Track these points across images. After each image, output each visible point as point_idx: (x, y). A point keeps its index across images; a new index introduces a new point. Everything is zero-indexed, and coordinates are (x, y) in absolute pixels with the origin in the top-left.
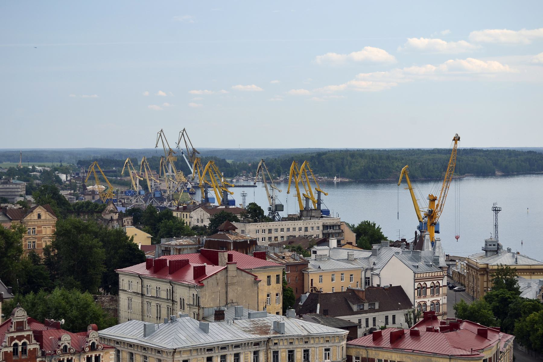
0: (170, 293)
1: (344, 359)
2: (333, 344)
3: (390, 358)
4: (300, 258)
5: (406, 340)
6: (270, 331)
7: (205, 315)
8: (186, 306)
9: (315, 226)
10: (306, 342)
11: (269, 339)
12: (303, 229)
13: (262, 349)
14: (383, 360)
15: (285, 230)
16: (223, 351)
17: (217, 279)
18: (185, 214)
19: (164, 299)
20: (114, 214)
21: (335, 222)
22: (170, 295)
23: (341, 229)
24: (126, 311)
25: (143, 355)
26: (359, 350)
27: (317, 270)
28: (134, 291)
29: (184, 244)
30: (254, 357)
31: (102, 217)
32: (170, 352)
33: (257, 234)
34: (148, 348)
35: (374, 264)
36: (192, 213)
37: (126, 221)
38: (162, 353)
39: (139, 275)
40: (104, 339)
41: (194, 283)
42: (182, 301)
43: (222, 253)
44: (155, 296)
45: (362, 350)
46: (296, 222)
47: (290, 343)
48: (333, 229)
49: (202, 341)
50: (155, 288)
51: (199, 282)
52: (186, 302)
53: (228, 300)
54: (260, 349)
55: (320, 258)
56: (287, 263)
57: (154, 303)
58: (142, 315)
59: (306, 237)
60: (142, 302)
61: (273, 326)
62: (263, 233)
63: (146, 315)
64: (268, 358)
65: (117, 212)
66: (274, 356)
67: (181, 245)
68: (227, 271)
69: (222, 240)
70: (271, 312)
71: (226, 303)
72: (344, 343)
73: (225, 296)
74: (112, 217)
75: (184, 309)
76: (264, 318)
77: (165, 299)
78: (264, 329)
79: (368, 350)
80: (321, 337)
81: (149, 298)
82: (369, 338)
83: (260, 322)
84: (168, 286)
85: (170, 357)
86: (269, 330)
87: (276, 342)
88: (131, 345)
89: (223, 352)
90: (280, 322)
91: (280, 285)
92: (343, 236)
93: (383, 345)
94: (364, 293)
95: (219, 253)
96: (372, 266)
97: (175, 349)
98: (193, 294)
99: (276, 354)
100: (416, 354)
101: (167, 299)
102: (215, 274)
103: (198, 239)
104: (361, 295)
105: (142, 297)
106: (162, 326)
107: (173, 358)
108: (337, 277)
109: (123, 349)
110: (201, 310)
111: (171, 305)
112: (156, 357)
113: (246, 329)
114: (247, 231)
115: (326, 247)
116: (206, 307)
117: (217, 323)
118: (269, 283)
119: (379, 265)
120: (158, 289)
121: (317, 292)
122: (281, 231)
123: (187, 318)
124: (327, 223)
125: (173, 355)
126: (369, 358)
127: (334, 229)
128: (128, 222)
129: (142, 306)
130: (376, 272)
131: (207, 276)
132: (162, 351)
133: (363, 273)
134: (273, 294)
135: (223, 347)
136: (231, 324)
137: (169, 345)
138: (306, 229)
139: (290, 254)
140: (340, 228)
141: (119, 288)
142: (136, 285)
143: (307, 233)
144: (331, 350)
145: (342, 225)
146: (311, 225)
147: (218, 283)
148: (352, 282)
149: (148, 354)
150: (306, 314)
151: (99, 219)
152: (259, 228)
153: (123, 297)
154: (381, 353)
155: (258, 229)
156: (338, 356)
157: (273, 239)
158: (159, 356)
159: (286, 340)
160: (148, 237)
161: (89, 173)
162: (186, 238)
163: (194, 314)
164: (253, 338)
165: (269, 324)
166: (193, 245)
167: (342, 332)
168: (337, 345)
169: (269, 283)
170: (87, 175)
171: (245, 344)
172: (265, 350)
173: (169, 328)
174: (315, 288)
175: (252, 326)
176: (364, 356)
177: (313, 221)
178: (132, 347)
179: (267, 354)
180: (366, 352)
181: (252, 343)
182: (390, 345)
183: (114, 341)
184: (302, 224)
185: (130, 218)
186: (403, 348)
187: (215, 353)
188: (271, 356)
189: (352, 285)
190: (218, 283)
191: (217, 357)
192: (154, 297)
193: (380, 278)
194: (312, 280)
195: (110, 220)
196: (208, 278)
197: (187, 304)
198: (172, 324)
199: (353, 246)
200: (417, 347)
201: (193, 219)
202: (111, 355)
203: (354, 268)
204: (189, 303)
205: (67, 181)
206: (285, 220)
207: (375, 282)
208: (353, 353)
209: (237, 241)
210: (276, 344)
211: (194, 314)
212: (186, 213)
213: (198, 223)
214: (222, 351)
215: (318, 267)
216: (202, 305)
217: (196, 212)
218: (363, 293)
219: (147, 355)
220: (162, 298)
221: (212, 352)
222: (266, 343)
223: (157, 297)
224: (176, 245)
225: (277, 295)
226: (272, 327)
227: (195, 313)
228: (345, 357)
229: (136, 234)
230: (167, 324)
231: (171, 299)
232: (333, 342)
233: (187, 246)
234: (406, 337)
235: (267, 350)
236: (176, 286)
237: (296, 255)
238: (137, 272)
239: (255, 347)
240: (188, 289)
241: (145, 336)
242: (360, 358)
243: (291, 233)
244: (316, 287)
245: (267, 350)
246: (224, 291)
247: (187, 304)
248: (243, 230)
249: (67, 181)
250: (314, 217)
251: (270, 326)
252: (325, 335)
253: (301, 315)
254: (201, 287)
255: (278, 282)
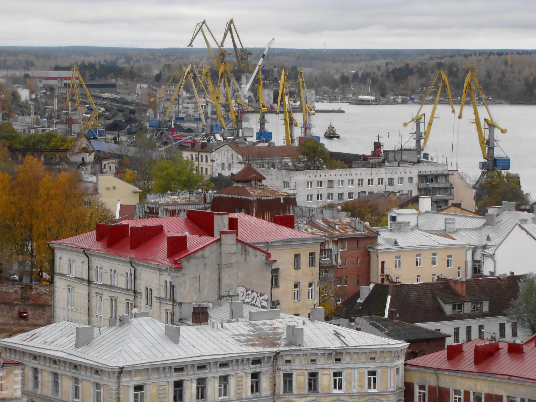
0: (131, 279)
1: (400, 388)
2: (381, 363)
3: (473, 387)
4: (365, 227)
5: (502, 358)
6: (279, 342)
7: (183, 316)
8: (154, 300)
9: (406, 177)
10: (338, 360)
11: (278, 353)
12: (366, 182)
13: (265, 369)
14: (462, 391)
15: (356, 182)
16: (202, 371)
17: (32, 257)
18: (204, 155)
19: (122, 288)
20: (88, 154)
21: (438, 170)
22: (131, 283)
23: (450, 181)
24: (64, 309)
25: (73, 377)
26: (424, 375)
27: (391, 247)
28: (77, 276)
29: (180, 202)
30: (252, 382)
31: (68, 159)
32: (114, 373)
33: (320, 187)
34: (80, 366)
35: (488, 239)
36: (213, 154)
37: (107, 165)
38: (102, 373)
39: (84, 251)
40: (15, 351)
41: (167, 263)
42: (149, 292)
43: (219, 217)
44: (109, 283)
45: (428, 375)
46: (375, 170)
47: (312, 361)
48: (437, 182)
49: (168, 356)
50: (109, 272)
51: (175, 262)
52: (155, 294)
53: (222, 292)
54: (262, 370)
55: (402, 227)
56: (343, 235)
57: (106, 295)
58: (89, 315)
59: (386, 194)
60: (89, 293)
61: (285, 334)
62: (310, 188)
63: (95, 315)
64: (275, 385)
65: (93, 151)
66: (285, 382)
67: (176, 204)
68: (221, 244)
69: (239, 197)
70: (300, 312)
71: (218, 296)
72: (402, 361)
73: (217, 285)
74: (83, 159)
75: (151, 305)
76: (274, 321)
77: (124, 289)
78: (271, 338)
79: (438, 375)
80: (354, 353)
81: (100, 287)
82: (442, 355)
83: (266, 327)
84: (128, 269)
85: (114, 380)
86: (279, 339)
87: (288, 358)
88: (55, 361)
89: (201, 374)
90: (296, 327)
91: (316, 269)
92: (453, 193)
93: (463, 367)
94: (464, 285)
95: (215, 216)
96: (485, 242)
97: (122, 368)
98: (166, 282)
99: (288, 377)
100: (515, 382)
101: (127, 290)
102: (201, 249)
103: (203, 195)
104: (459, 289)
105: (89, 286)
106: (107, 331)
107: (119, 383)
108: (426, 259)
109: (44, 368)
110: (177, 307)
111: (132, 298)
112: (92, 380)
113: (242, 338)
114: (292, 184)
115: (413, 211)
116: (185, 301)
117: (196, 327)
118: (297, 266)
119: (496, 240)
120: (113, 273)
121: (392, 282)
122: (318, 186)
123: (145, 318)
124: (425, 172)
125: (119, 377)
126: (440, 388)
127: (438, 182)
128: (110, 167)
129: (89, 301)
130: (489, 251)
131: (188, 251)
132: (102, 370)
133: (470, 253)
134: (304, 284)
135: (201, 365)
136: (218, 328)
137: (113, 361)
138: (361, 182)
139: (348, 220)
140: (447, 181)
141: (55, 272)
142: (80, 266)
143: (390, 189)
144: (344, 374)
145: (451, 175)
146: (399, 175)
147: (205, 264)
148: (434, 266)
149: (81, 375)
150: (360, 316)
151: (63, 162)
152: (312, 178)
153: (60, 284)
154: (459, 380)
155: (310, 180)
156: (389, 383)
157: (335, 197)
158: (96, 378)
159: (305, 356)
160: (135, 192)
161: (69, 87)
162: (185, 194)
163: (167, 313)
164: (251, 351)
165: (280, 331)
166: (195, 204)
167: (397, 344)
168: (389, 365)
169: (297, 266)
170: (66, 91)
171: (237, 361)
172: (270, 372)
173: (117, 334)
174: (387, 276)
175: (251, 333)
176: (433, 383)
177: (401, 169)
178: (57, 365)
179: (274, 377)
180: (436, 378)
181: (249, 359)
182: (474, 366)
183: (30, 354)
184: (384, 173)
185: (114, 161)
186: (495, 372)
187: (188, 375)
188: (280, 381)
189: (450, 273)
190: (205, 264)
191: (191, 382)
192: (106, 285)
193: (494, 261)
194: (383, 263)
195: (81, 164)
196: (189, 255)
197: (156, 297)
198: (122, 327)
199: (462, 209)
200: (512, 371)
201: (214, 164)
202: (16, 375)
203: (454, 245)
204: (158, 296)
205: (31, 100)
206: (357, 167)
207: (487, 269)
208: (416, 379)
209: (263, 198)
210: (288, 361)
211: (167, 313)
212: (206, 154)
213: (223, 171)
214: (199, 372)
215: (394, 242)
216: (178, 299)
217: (220, 153)
218: (463, 286)
219: (80, 377)
220: (119, 288)
221: (183, 373)
222: (272, 359)
223: (111, 286)
224: (168, 204)
225: (310, 285)
226: (284, 336)
227: (169, 312)
228: (402, 385)
229: (115, 187)
230: (114, 328)
231: (133, 289)
232: (382, 360)
233: (176, 206)
234: (502, 354)
235: (274, 372)
236: (139, 268)
237: (357, 222)
238: (78, 244)
239: (254, 366)
240: (158, 272)
241: (77, 346)
242: (427, 388)
243: (366, 188)
244: (389, 275)
245: (274, 372)
246: (215, 276)
247: (156, 297)
248: (287, 182)
249: (31, 100)
250: (405, 162)
251: (282, 334)
252: (368, 350)
253: (352, 318)
254: (178, 269)
255: (312, 263)
